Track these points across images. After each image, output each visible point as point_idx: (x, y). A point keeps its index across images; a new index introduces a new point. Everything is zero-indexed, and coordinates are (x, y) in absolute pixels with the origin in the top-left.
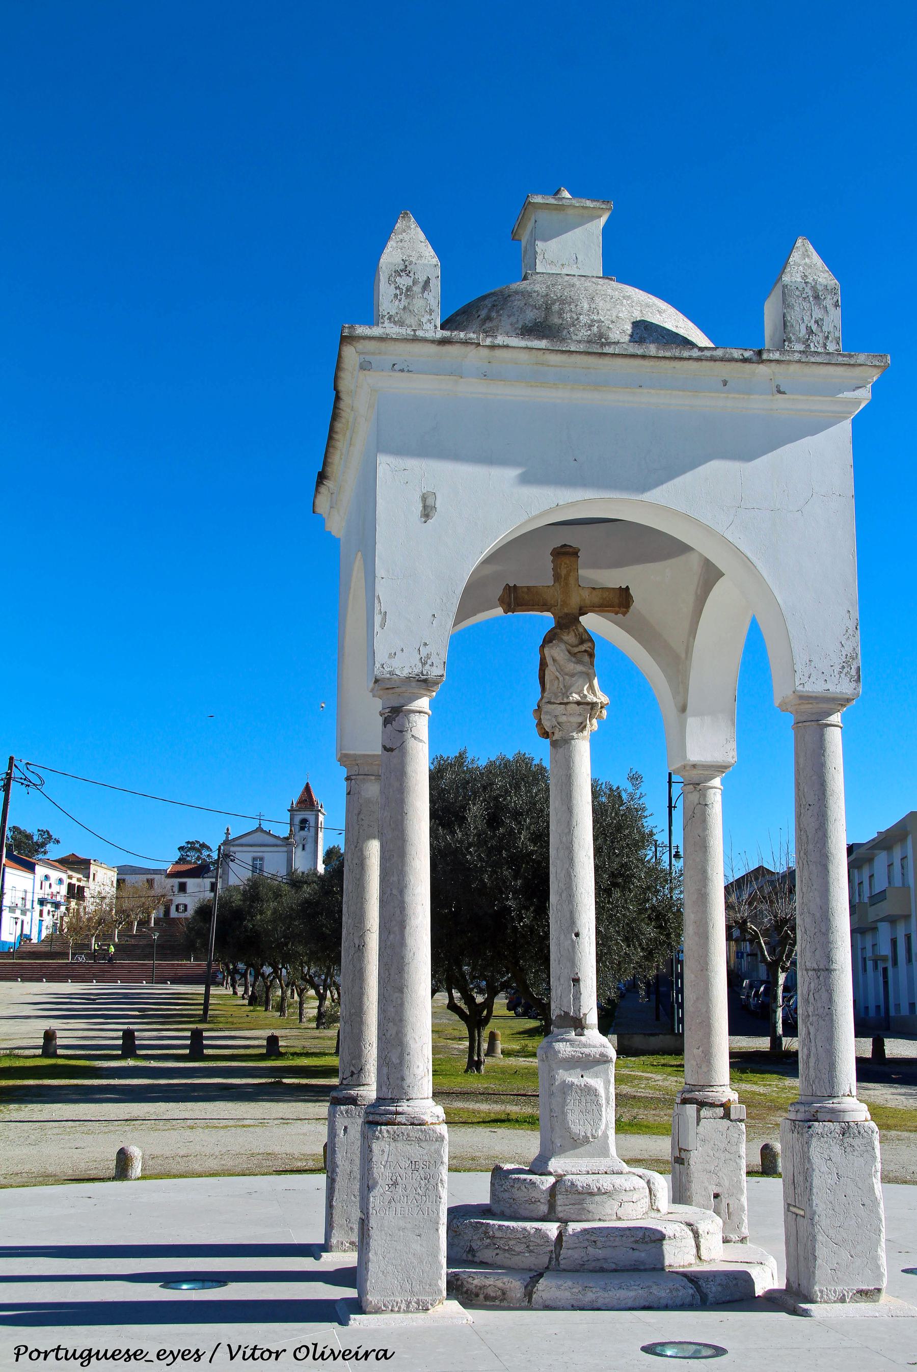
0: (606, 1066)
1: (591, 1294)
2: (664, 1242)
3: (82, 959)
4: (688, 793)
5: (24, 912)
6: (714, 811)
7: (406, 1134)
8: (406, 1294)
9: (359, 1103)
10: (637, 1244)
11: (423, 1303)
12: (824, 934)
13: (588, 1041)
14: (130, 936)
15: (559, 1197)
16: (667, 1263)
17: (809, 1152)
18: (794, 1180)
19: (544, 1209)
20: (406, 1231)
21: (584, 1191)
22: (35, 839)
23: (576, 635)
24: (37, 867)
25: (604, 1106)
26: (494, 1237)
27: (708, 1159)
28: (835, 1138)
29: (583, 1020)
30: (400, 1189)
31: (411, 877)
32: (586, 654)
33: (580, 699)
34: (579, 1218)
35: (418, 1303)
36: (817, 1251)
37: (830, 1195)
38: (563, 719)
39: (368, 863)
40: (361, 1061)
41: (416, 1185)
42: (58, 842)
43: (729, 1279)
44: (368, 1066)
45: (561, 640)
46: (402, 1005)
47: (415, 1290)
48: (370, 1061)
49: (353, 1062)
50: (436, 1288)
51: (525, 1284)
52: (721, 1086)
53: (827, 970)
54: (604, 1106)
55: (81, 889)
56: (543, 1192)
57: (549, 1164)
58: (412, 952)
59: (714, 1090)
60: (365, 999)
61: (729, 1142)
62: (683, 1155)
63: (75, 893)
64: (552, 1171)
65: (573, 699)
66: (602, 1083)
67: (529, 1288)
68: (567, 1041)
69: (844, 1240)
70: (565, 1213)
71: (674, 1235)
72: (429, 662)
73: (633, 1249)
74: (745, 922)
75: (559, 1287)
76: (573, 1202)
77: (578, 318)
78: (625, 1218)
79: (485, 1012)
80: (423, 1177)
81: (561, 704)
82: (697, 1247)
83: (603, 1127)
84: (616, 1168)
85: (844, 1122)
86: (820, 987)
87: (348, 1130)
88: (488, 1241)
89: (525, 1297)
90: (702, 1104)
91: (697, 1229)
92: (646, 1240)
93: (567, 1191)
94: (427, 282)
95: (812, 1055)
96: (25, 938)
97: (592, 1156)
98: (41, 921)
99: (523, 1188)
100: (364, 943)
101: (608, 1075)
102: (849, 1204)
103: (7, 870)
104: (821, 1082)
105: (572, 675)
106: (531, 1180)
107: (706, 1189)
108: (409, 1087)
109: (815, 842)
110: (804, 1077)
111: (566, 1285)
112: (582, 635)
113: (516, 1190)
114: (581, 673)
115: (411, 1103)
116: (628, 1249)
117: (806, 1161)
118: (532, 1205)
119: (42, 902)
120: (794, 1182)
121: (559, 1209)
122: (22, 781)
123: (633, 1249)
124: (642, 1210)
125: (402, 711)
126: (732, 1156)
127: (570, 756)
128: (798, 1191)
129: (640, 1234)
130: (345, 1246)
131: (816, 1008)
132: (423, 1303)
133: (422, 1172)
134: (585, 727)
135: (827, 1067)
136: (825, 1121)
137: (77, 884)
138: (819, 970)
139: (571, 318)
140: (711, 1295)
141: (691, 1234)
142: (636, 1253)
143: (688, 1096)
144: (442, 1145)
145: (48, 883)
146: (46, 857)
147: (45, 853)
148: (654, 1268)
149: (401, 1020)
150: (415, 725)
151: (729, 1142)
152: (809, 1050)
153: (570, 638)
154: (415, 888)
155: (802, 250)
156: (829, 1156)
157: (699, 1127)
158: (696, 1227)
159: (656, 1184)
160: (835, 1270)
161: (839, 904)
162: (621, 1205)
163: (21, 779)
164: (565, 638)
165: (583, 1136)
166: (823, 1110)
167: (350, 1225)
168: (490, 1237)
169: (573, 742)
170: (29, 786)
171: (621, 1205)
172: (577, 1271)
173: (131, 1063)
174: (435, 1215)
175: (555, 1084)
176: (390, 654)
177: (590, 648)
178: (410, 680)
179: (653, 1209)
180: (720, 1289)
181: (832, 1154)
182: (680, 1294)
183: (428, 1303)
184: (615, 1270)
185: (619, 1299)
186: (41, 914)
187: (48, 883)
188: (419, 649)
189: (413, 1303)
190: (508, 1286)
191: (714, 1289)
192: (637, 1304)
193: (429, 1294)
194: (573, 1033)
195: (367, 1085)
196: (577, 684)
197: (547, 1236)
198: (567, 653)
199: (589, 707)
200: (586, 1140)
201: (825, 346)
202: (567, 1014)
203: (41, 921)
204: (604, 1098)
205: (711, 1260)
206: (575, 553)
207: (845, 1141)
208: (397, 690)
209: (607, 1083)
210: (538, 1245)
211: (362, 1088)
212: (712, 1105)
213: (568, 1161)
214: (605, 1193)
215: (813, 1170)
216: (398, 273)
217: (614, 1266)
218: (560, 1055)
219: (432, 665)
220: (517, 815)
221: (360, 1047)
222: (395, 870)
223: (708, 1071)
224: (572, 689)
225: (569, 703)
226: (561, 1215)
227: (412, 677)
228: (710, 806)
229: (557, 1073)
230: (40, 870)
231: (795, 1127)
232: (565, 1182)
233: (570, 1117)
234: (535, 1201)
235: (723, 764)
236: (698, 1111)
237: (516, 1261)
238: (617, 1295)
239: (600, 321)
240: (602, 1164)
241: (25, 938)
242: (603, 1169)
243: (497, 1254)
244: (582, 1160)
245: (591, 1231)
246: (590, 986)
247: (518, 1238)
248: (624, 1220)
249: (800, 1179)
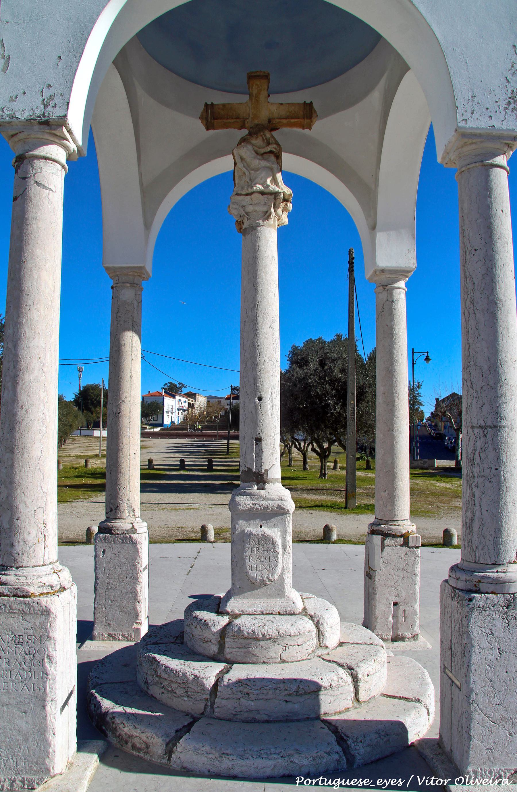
0: (283, 517)
1: (227, 761)
2: (321, 693)
3: (192, 430)
4: (379, 293)
5: (172, 413)
6: (399, 306)
7: (8, 606)
8: (10, 772)
9: (114, 532)
10: (290, 697)
11: (29, 782)
12: (492, 388)
13: (267, 494)
14: (211, 422)
15: (227, 640)
16: (322, 711)
17: (468, 627)
18: (451, 646)
19: (214, 649)
20: (10, 706)
21: (250, 637)
22: (178, 386)
23: (263, 140)
24: (176, 396)
25: (281, 553)
27: (390, 577)
28: (498, 611)
29: (264, 475)
31: (26, 329)
32: (272, 155)
33: (263, 188)
34: (244, 661)
35: (23, 782)
36: (472, 730)
37: (490, 672)
38: (250, 209)
39: (123, 350)
40: (117, 501)
41: (21, 660)
42: (186, 387)
43: (380, 737)
44: (123, 505)
45: (250, 143)
46: (12, 466)
47: (20, 768)
48: (124, 501)
49: (112, 501)
50: (43, 767)
51: (168, 740)
52: (402, 520)
53: (495, 427)
54: (281, 553)
55: (193, 405)
56: (214, 634)
57: (228, 604)
58: (25, 409)
59: (396, 524)
60: (121, 454)
61: (407, 564)
62: (371, 572)
63: (191, 406)
64: (229, 610)
65: (256, 189)
66: (279, 533)
67: (170, 745)
68: (248, 494)
69: (503, 718)
70: (232, 655)
71: (331, 685)
72: (52, 103)
73: (286, 701)
74: (445, 412)
75: (196, 750)
76: (239, 645)
78: (289, 660)
79: (327, 453)
80: (28, 651)
81: (247, 195)
82: (355, 690)
83: (279, 571)
84: (289, 609)
85: (509, 594)
86: (486, 445)
87: (106, 552)
88: (157, 679)
89: (165, 754)
90: (386, 535)
91: (357, 674)
92: (300, 692)
93: (234, 635)
95: (476, 519)
96: (173, 423)
97: (269, 596)
98: (179, 416)
99: (198, 627)
100: (120, 411)
101: (285, 525)
102: (510, 680)
103: (165, 397)
104: (486, 550)
105: (257, 170)
106: (205, 621)
107: (387, 599)
108: (19, 554)
109: (482, 289)
110: (466, 542)
111: (203, 749)
112: (269, 140)
113: (194, 628)
114: (265, 168)
115: (20, 572)
116: (281, 702)
117: (465, 635)
118: (205, 644)
119: (179, 409)
120: (451, 648)
121: (227, 650)
123: (286, 701)
124: (307, 651)
125: (26, 158)
126: (409, 575)
127: (256, 241)
128: (455, 659)
129: (294, 688)
130: (104, 636)
131: (482, 468)
132: (29, 782)
133: (27, 647)
134: (270, 215)
135: (492, 533)
136: (487, 593)
137: (192, 403)
138: (486, 427)
140: (358, 757)
141: (349, 679)
142: (290, 706)
143: (375, 528)
144: (48, 619)
145: (180, 402)
146: (182, 393)
147: (182, 391)
148: (308, 718)
149: (11, 483)
150: (39, 171)
151: (407, 564)
152: (473, 513)
154: (30, 341)
156: (490, 630)
157: (383, 553)
158: (356, 671)
159: (325, 624)
160: (491, 749)
161: (508, 355)
162: (286, 648)
164: (254, 141)
165: (260, 580)
166: (486, 580)
167: (108, 622)
168: (158, 676)
169: (259, 228)
171: (286, 648)
172: (230, 720)
173: (182, 472)
174: (42, 691)
175: (235, 533)
176: (11, 98)
178: (31, 123)
179: (321, 647)
180: (368, 749)
181: (494, 628)
182: (324, 761)
183: (34, 782)
184: (267, 722)
185: (257, 768)
186: (178, 413)
187: (180, 402)
188: (42, 92)
189: (18, 782)
190: (150, 741)
191: (362, 750)
192: (276, 773)
193: (35, 772)
194: (256, 488)
195: (122, 518)
196: (260, 177)
197: (202, 685)
198: (254, 153)
199: (272, 197)
200: (263, 583)
202: (250, 470)
203: (179, 416)
204: (280, 547)
205: (370, 699)
207: (510, 613)
208: (21, 136)
209: (284, 532)
210: (195, 692)
211: (117, 521)
212: (394, 536)
213: (245, 600)
214: (270, 639)
215: (472, 646)
217: (265, 718)
218: (240, 508)
219: (55, 106)
220: (334, 361)
221: (117, 490)
222: (11, 322)
223: (392, 509)
224: (256, 180)
225: (253, 193)
226: (228, 656)
227: (32, 119)
228: (396, 302)
229: (237, 523)
230: (177, 398)
231: (455, 595)
232: (233, 627)
233: (248, 563)
234: (207, 641)
235: (406, 269)
236: (383, 541)
237: (176, 703)
238: (255, 764)
240: (277, 604)
241: (173, 423)
242: (277, 609)
243: (163, 693)
244: (259, 600)
245: (245, 682)
246: (272, 445)
247: (179, 683)
248: (288, 662)
249: (458, 649)
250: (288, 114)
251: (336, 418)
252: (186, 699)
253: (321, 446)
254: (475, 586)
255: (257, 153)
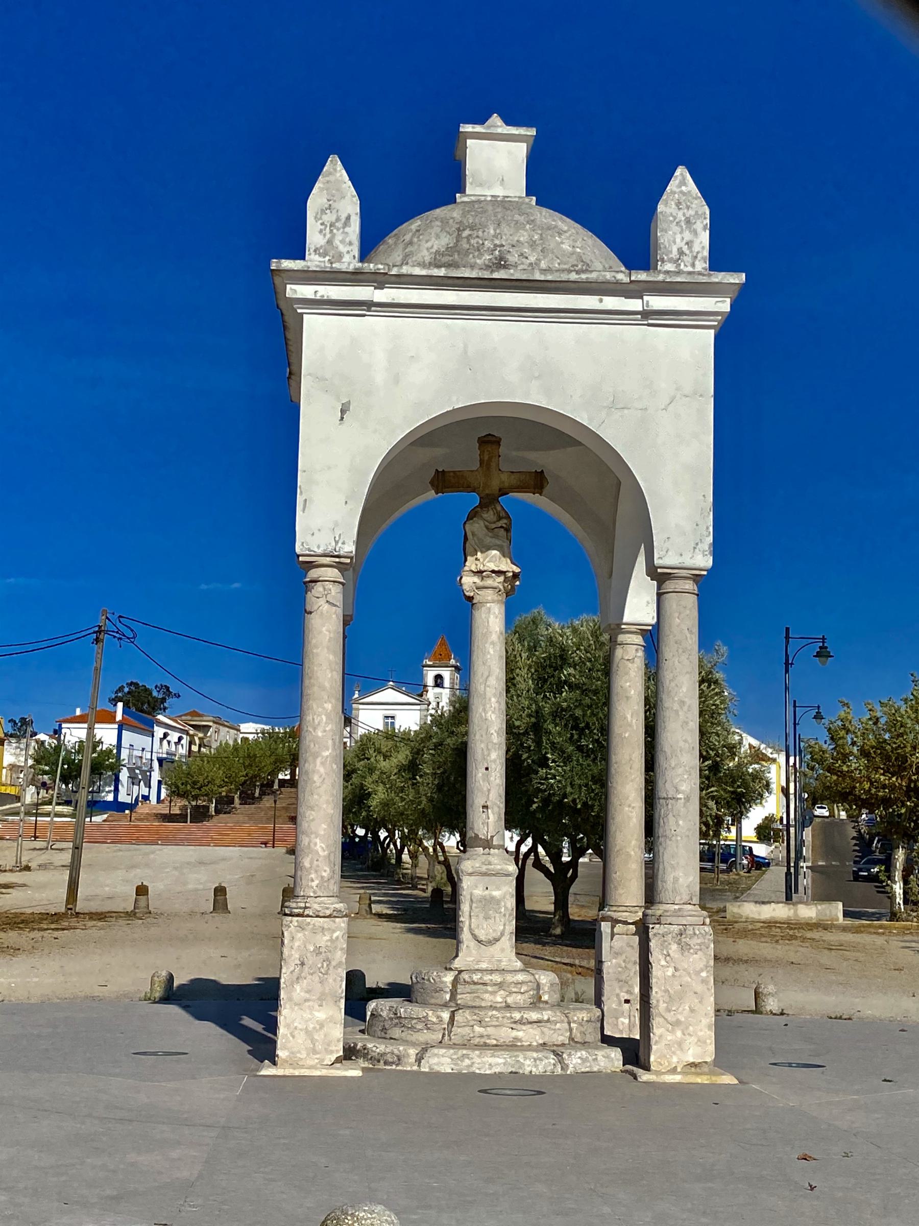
15: (459, 986)
26: (401, 1017)
30: (306, 968)
32: (502, 530)
77: (483, 244)
94: (348, 218)
107: (618, 995)
122: (115, 634)
123: (512, 1029)
139: (478, 243)
153: (489, 515)
155: (680, 178)
163: (113, 632)
164: (485, 516)
170: (120, 639)
177: (506, 524)
198: (485, 529)
201: (693, 265)
206: (497, 442)
216: (323, 212)
219: (343, 543)
236: (613, 927)
239: (502, 246)
250: (519, 483)
251: (743, 803)
252: (425, 1031)
253: (555, 856)
254: (658, 919)
255: (487, 527)
